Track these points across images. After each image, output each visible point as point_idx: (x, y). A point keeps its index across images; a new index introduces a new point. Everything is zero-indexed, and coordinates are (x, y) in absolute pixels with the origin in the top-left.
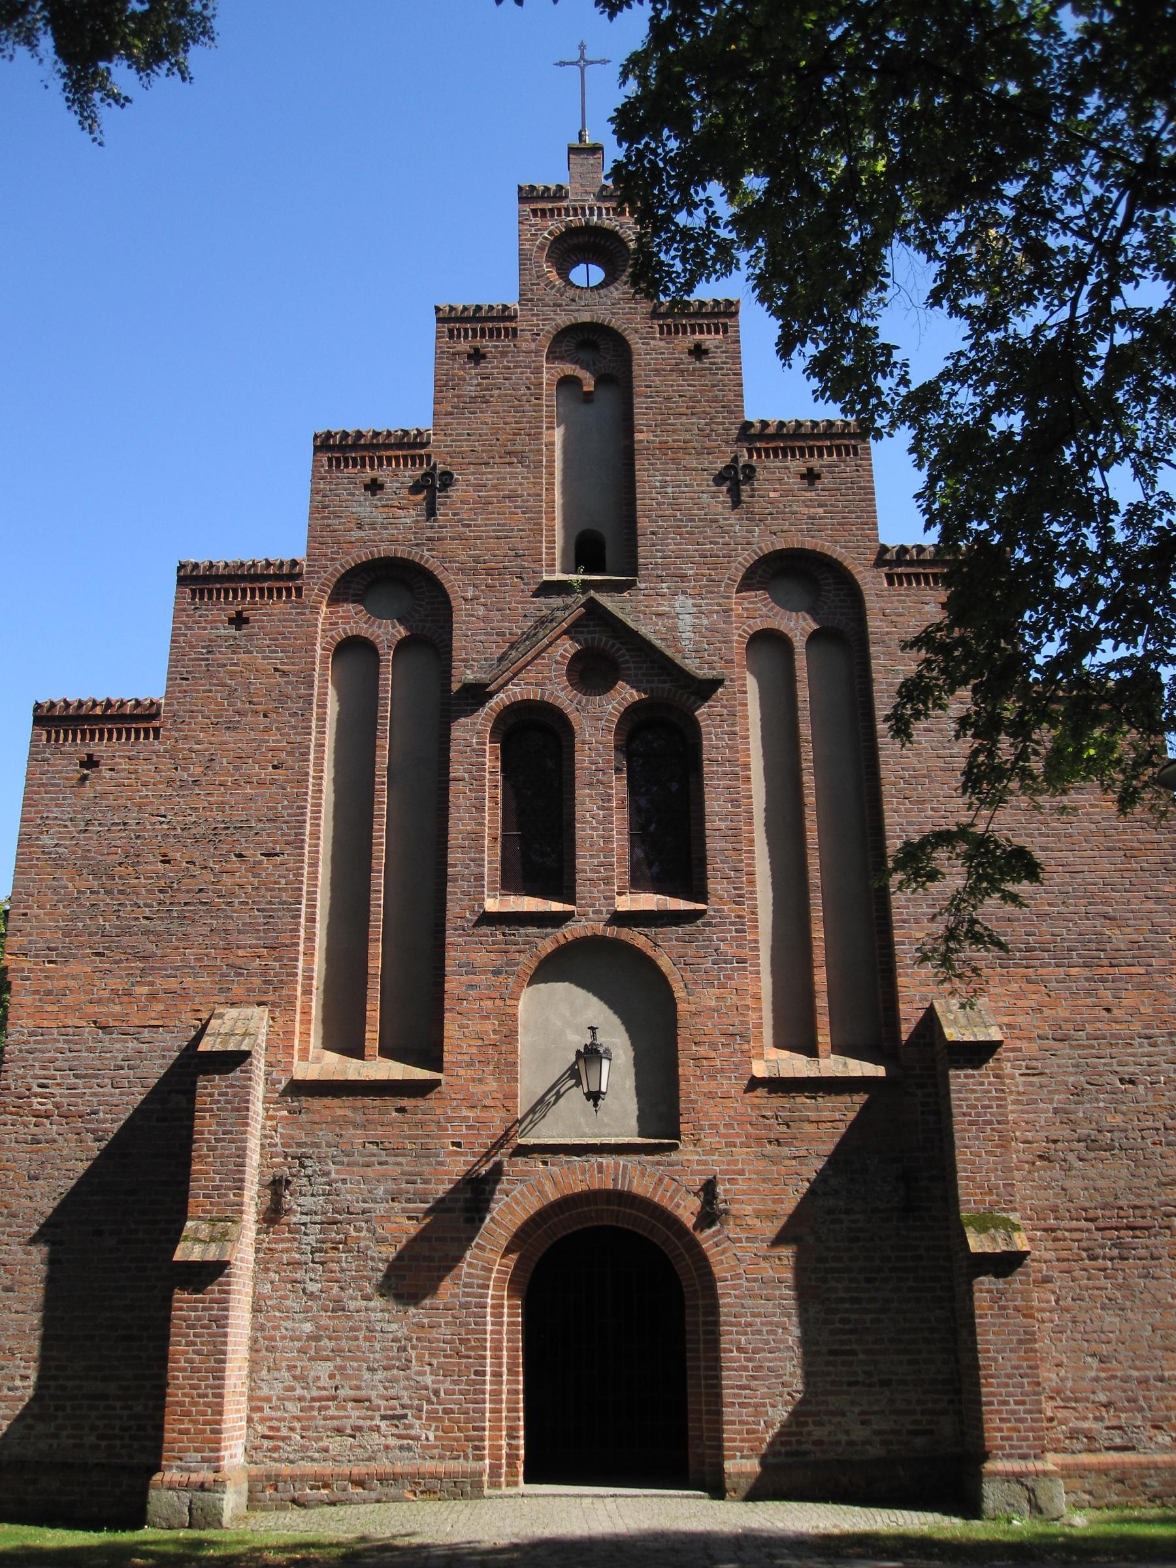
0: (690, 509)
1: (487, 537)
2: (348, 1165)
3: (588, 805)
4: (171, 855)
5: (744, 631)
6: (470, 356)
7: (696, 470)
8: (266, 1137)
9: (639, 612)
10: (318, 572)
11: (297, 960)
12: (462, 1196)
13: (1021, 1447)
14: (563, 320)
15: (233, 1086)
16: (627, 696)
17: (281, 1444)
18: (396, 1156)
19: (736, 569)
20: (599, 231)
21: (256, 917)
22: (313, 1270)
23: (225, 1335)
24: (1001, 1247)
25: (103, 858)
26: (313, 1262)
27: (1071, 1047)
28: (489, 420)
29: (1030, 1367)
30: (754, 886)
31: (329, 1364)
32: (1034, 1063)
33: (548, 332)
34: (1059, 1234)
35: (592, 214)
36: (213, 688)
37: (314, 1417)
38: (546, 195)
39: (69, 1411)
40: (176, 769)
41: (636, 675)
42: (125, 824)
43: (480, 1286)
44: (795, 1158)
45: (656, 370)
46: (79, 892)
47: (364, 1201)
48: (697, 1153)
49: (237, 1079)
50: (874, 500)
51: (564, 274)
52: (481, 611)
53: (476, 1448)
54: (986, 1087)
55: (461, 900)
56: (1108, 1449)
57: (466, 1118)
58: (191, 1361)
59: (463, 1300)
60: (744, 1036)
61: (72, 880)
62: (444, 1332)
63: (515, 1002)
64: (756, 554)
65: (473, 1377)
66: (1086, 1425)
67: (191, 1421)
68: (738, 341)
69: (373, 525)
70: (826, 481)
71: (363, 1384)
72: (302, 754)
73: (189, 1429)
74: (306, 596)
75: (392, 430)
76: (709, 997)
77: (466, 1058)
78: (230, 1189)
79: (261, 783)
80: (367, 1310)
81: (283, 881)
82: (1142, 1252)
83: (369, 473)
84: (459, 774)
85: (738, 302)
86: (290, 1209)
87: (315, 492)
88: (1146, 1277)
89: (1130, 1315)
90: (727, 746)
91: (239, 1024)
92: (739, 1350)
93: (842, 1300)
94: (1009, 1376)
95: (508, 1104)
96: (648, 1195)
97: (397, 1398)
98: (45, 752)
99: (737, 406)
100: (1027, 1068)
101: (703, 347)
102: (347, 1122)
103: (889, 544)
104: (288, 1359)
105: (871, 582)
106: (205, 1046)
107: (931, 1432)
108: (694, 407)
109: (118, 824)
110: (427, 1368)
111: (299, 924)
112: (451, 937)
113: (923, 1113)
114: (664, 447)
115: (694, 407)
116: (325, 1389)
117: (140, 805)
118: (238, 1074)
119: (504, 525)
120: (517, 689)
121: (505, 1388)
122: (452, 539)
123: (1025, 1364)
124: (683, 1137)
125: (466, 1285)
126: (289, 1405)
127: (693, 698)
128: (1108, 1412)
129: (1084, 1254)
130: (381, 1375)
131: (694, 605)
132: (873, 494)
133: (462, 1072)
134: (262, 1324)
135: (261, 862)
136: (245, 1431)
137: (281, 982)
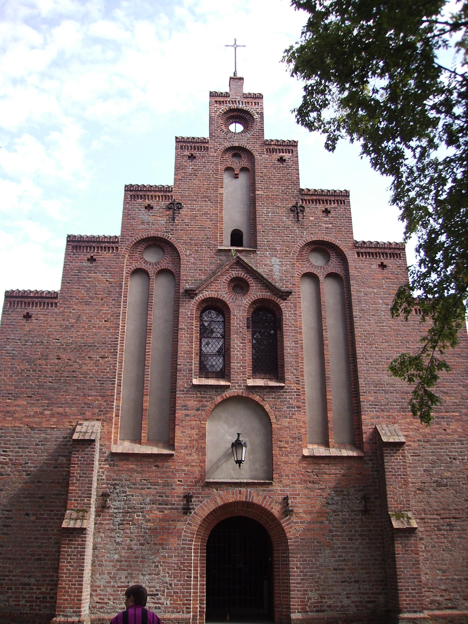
0: (278, 222)
1: (195, 230)
2: (134, 489)
3: (236, 341)
4: (61, 356)
5: (300, 273)
6: (189, 157)
7: (281, 207)
8: (99, 476)
9: (257, 263)
10: (125, 241)
11: (114, 402)
12: (182, 503)
13: (414, 608)
14: (227, 145)
15: (87, 454)
16: (252, 297)
17: (105, 606)
18: (155, 485)
19: (297, 247)
20: (241, 111)
21: (96, 383)
22: (119, 532)
23: (84, 559)
24: (406, 526)
25: (32, 356)
26: (119, 529)
27: (431, 445)
28: (197, 183)
29: (417, 575)
30: (303, 377)
31: (125, 572)
32: (416, 451)
33: (221, 149)
34: (426, 520)
35: (239, 104)
36: (80, 287)
37: (119, 594)
38: (221, 95)
39: (13, 590)
40: (64, 320)
41: (256, 289)
42: (42, 342)
43: (189, 541)
44: (320, 489)
45: (265, 166)
46: (22, 370)
47: (141, 504)
48: (280, 486)
49: (89, 451)
50: (351, 222)
51: (227, 126)
52: (192, 260)
53: (187, 608)
54: (399, 460)
55: (183, 379)
56: (446, 608)
57: (184, 470)
58: (69, 570)
59: (182, 546)
60: (300, 439)
61: (19, 365)
62: (175, 559)
63: (205, 422)
64: (305, 242)
65: (186, 578)
66: (437, 598)
67: (68, 595)
68: (298, 157)
69: (148, 223)
70: (333, 213)
71: (140, 581)
72: (117, 316)
73: (68, 599)
74: (120, 251)
75: (157, 185)
76: (285, 422)
77: (184, 445)
78: (86, 497)
79: (100, 328)
80: (142, 549)
81: (108, 369)
82: (458, 528)
83: (147, 202)
84: (183, 327)
85: (298, 141)
86: (110, 506)
87: (124, 209)
88: (460, 538)
89: (454, 553)
90: (293, 319)
91: (89, 428)
92: (297, 568)
93: (339, 548)
94: (409, 578)
95: (201, 464)
96: (260, 504)
97: (154, 587)
98: (9, 311)
99: (297, 182)
100: (413, 453)
101: (283, 158)
102: (133, 470)
103: (358, 240)
104: (108, 570)
105: (351, 256)
106: (75, 436)
107: (375, 602)
108: (280, 182)
109: (39, 342)
110: (167, 575)
111: (114, 387)
112: (179, 395)
113: (372, 471)
114: (268, 197)
115: (280, 182)
116: (123, 582)
117: (48, 335)
118: (89, 449)
119: (203, 225)
120: (207, 293)
121: (199, 583)
122: (181, 230)
123: (415, 573)
124: (274, 480)
125: (183, 540)
126: (108, 589)
127: (279, 299)
128: (445, 593)
129: (436, 529)
130: (147, 577)
131: (280, 261)
132: (351, 220)
133: (182, 451)
134: (97, 555)
135: (99, 360)
136: (89, 600)
137: (107, 411)
